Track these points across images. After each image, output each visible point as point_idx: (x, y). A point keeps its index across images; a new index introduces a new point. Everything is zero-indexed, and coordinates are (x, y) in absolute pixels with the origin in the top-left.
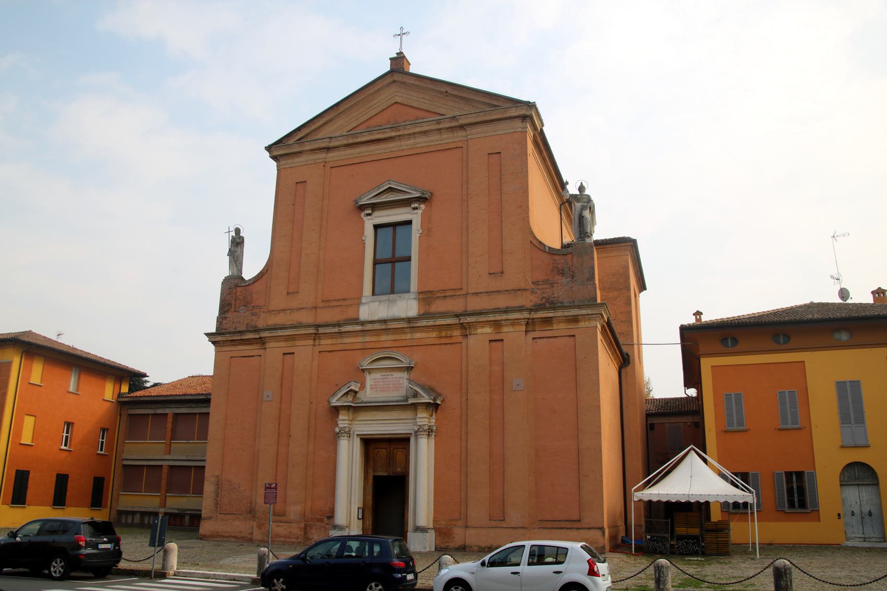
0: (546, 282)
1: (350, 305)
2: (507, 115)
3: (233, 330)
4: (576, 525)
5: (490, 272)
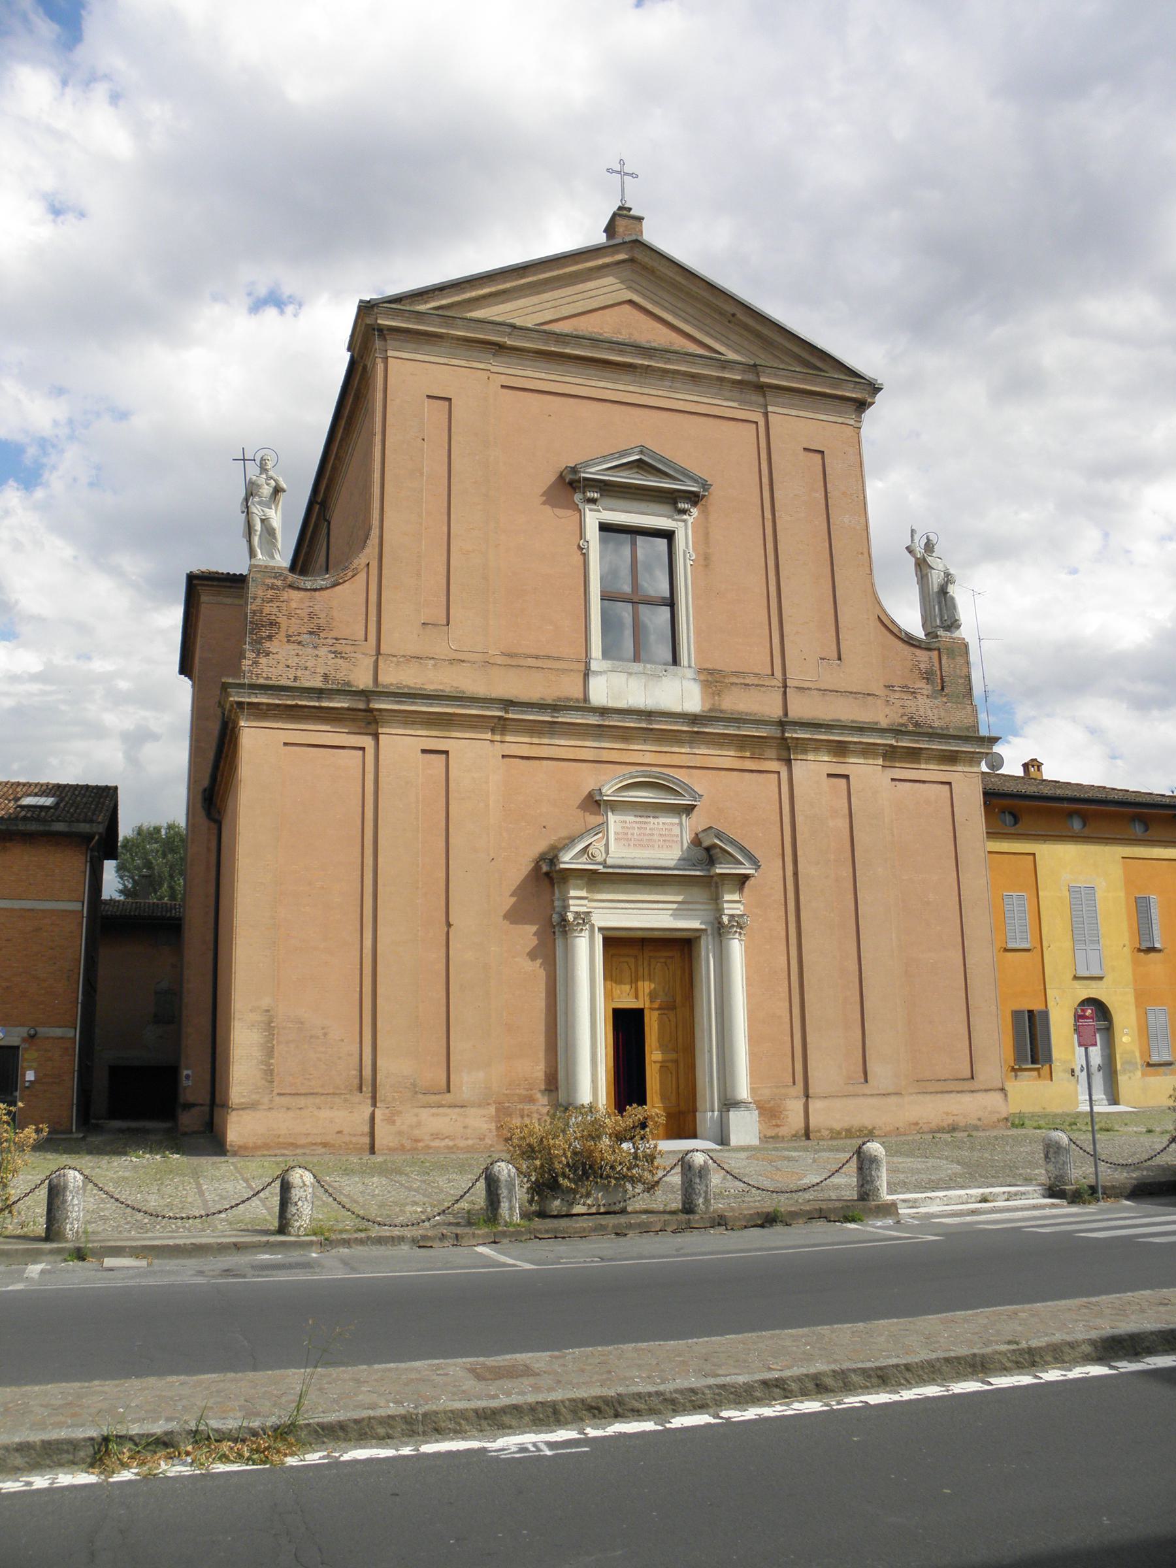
1: (565, 671)
4: (967, 1085)
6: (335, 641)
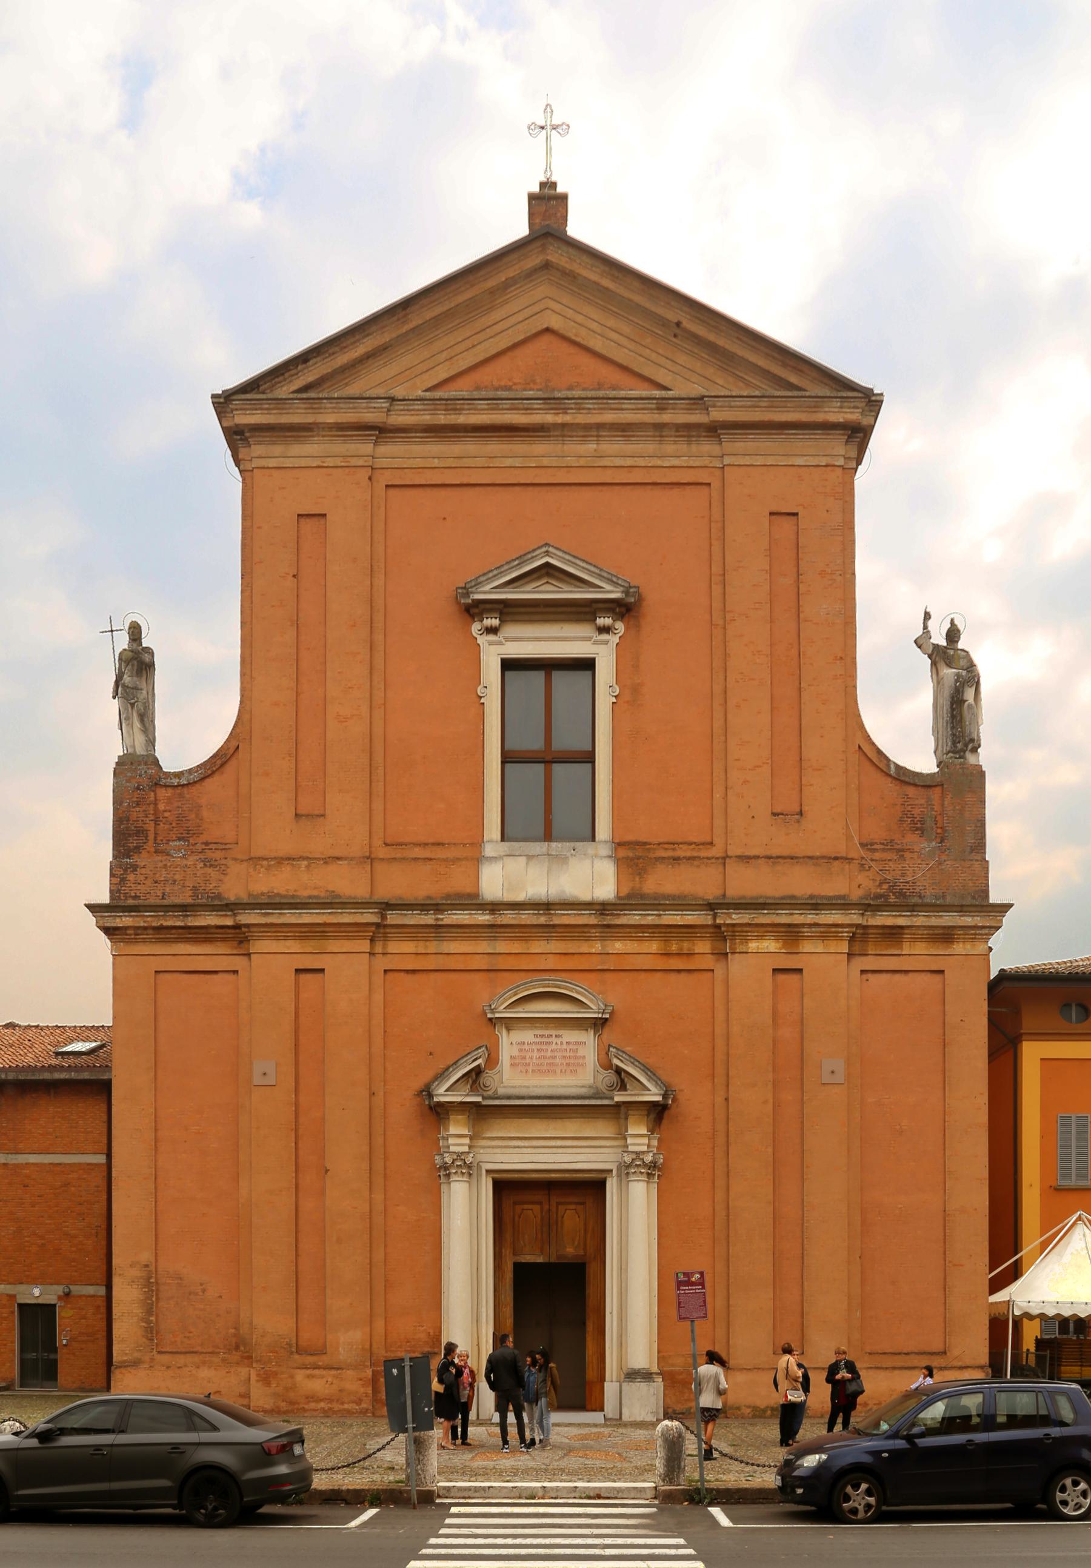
0: (889, 845)
1: (456, 860)
2: (820, 417)
3: (159, 902)
5: (775, 811)
6: (204, 847)
